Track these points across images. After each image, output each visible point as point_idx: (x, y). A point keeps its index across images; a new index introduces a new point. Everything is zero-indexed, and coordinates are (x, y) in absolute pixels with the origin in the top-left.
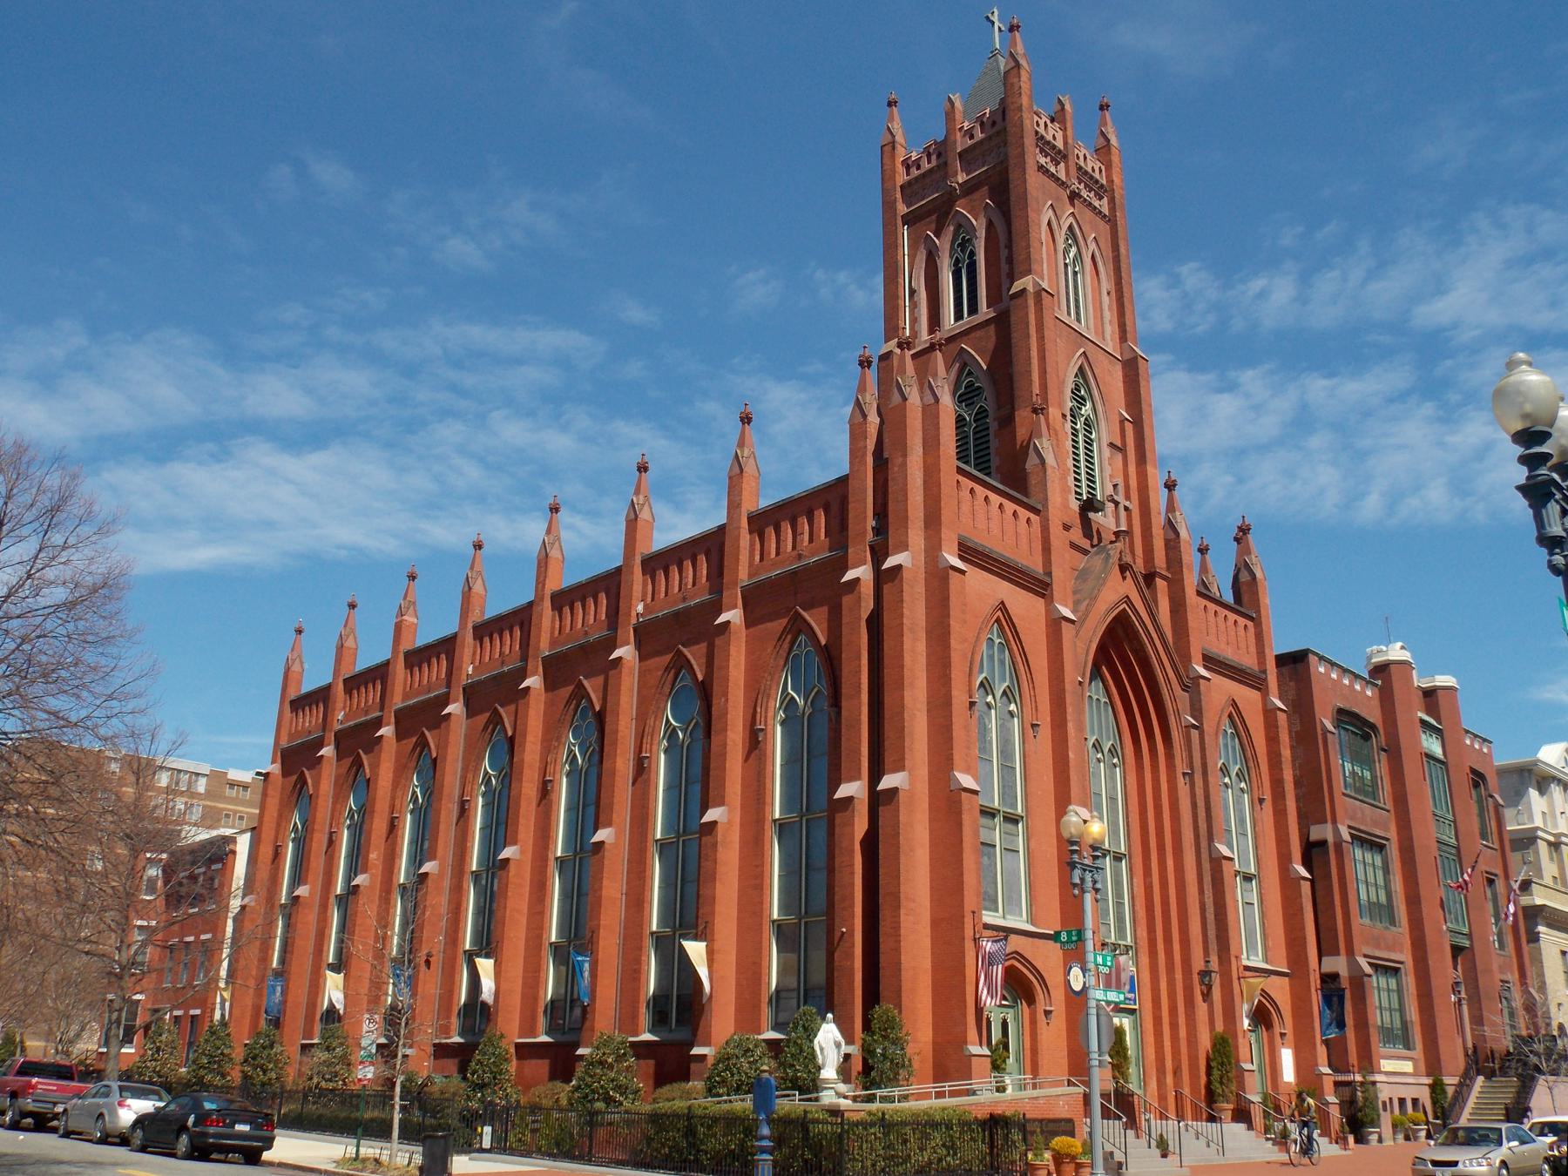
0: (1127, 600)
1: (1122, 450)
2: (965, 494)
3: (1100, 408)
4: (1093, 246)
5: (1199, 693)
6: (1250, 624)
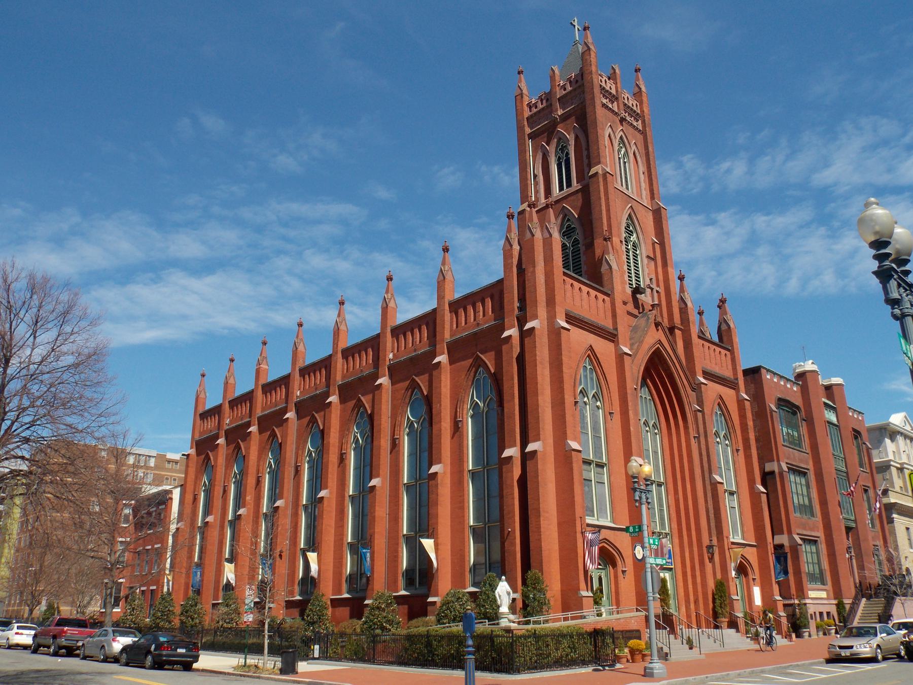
0: (660, 342)
3: (641, 236)
4: (634, 147)
6: (728, 353)
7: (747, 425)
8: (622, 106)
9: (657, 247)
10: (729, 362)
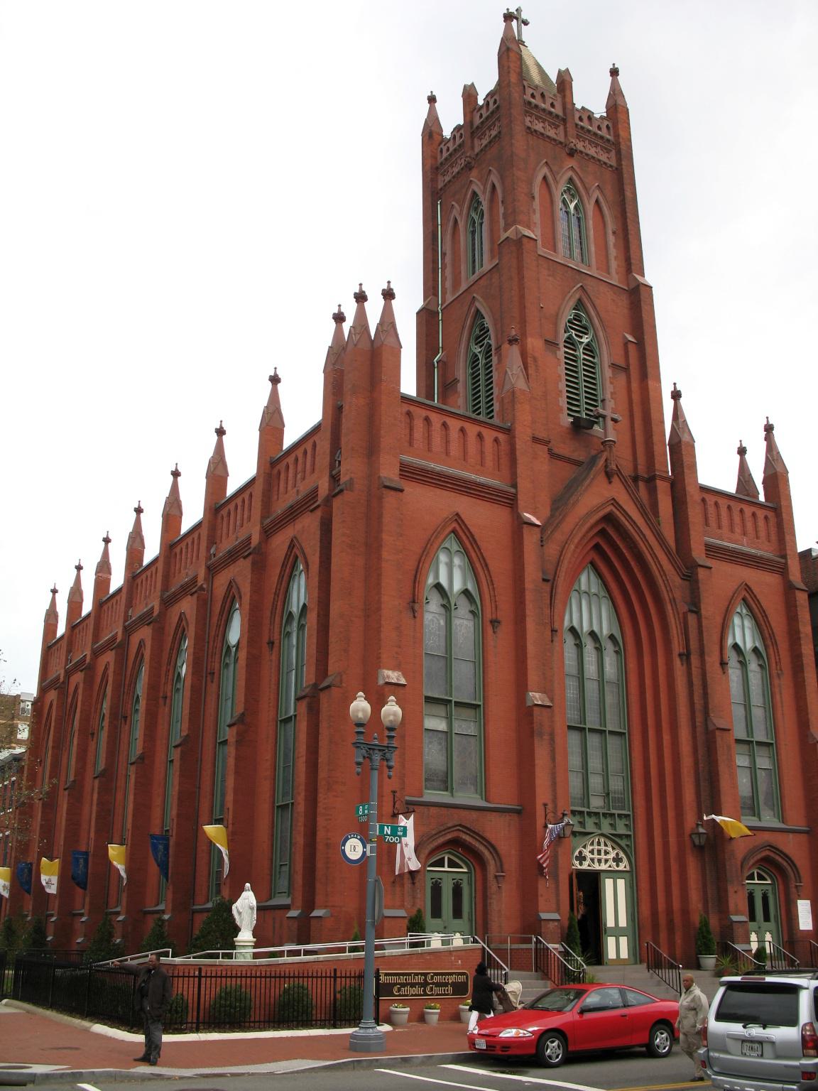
0: (614, 502)
1: (626, 370)
2: (419, 425)
3: (601, 334)
4: (597, 194)
5: (697, 581)
6: (501, 437)
7: (798, 632)
8: (572, 131)
9: (632, 350)
10: (773, 531)
